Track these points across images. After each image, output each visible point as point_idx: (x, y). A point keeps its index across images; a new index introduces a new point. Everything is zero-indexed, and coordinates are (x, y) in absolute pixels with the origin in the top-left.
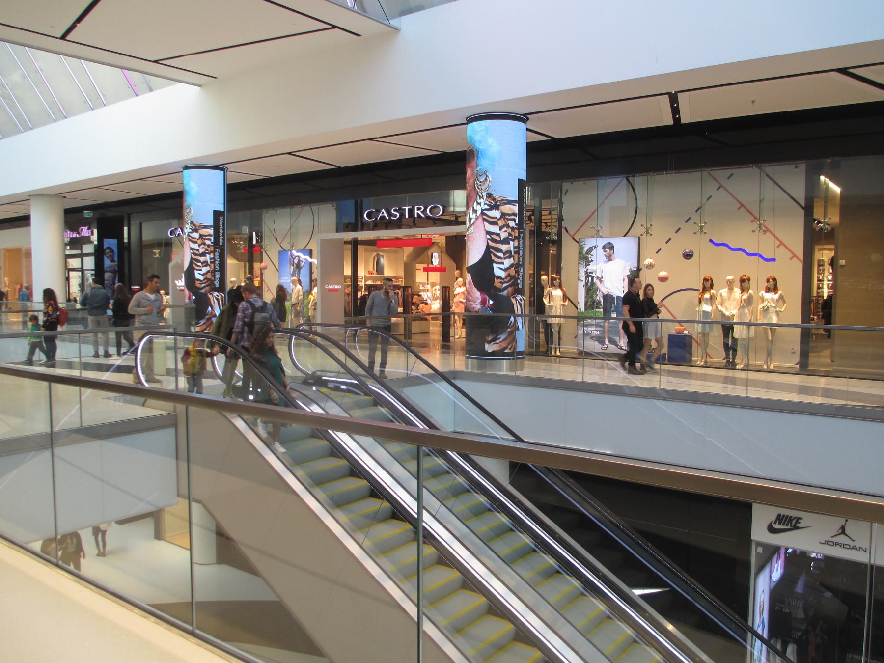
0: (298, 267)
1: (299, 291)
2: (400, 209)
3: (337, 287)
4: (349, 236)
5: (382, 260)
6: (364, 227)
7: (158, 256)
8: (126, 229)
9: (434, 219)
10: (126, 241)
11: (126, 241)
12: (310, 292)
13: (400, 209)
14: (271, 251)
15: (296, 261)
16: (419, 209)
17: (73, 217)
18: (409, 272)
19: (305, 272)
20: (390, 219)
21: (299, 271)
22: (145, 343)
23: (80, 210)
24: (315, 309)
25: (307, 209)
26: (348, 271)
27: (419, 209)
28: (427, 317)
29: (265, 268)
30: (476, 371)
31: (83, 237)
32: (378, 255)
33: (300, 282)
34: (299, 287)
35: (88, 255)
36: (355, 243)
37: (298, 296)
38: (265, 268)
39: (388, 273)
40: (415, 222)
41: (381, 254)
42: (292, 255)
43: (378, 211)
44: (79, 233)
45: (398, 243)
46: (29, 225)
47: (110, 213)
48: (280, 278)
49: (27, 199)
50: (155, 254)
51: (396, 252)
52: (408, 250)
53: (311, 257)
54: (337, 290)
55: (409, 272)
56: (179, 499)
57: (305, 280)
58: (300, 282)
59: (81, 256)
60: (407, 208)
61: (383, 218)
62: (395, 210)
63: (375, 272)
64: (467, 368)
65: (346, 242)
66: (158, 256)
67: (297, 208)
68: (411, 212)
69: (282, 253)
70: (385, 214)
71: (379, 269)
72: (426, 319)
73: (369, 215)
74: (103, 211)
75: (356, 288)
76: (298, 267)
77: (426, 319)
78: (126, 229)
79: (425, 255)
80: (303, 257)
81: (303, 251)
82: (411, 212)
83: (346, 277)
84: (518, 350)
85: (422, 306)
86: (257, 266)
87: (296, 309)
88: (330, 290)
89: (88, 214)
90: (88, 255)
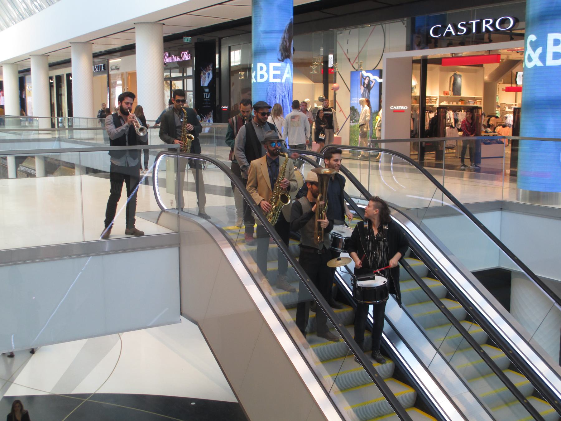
0: (368, 87)
1: (366, 112)
2: (467, 23)
3: (403, 108)
4: (418, 54)
5: (459, 80)
6: (435, 44)
7: (243, 77)
8: (217, 56)
9: (504, 33)
10: (217, 66)
11: (217, 66)
12: (377, 113)
13: (467, 23)
14: (344, 73)
15: (366, 82)
16: (487, 22)
17: (171, 43)
18: (489, 91)
19: (374, 92)
20: (456, 35)
21: (369, 92)
22: (161, 161)
23: (178, 37)
24: (380, 130)
25: (378, 27)
26: (417, 92)
27: (487, 22)
28: (503, 140)
29: (337, 89)
30: (527, 203)
31: (184, 61)
32: (455, 74)
33: (368, 102)
34: (366, 108)
35: (189, 77)
36: (424, 62)
37: (365, 117)
38: (337, 89)
39: (465, 93)
40: (480, 38)
41: (458, 73)
42: (362, 76)
43: (445, 27)
44: (181, 58)
45: (476, 62)
46: (134, 53)
47: (206, 38)
48: (351, 99)
49: (129, 28)
50: (241, 76)
51: (476, 71)
52: (490, 68)
53: (381, 77)
54: (402, 111)
55: (489, 91)
56: (182, 317)
57: (374, 100)
58: (368, 102)
59: (183, 79)
60: (474, 22)
61: (449, 33)
62: (462, 25)
63: (451, 93)
64: (518, 199)
65: (415, 62)
66: (243, 77)
67: (368, 28)
68: (479, 25)
69: (354, 74)
70: (452, 30)
71: (456, 89)
72: (502, 143)
73: (435, 32)
74: (200, 37)
75: (424, 109)
76: (368, 87)
77: (502, 143)
78: (217, 56)
79: (509, 73)
80: (372, 77)
81: (373, 71)
82: (479, 25)
83: (415, 98)
84: (207, 196)
85: (499, 128)
86: (331, 86)
87: (362, 130)
88: (395, 111)
89: (187, 39)
90: (189, 77)
